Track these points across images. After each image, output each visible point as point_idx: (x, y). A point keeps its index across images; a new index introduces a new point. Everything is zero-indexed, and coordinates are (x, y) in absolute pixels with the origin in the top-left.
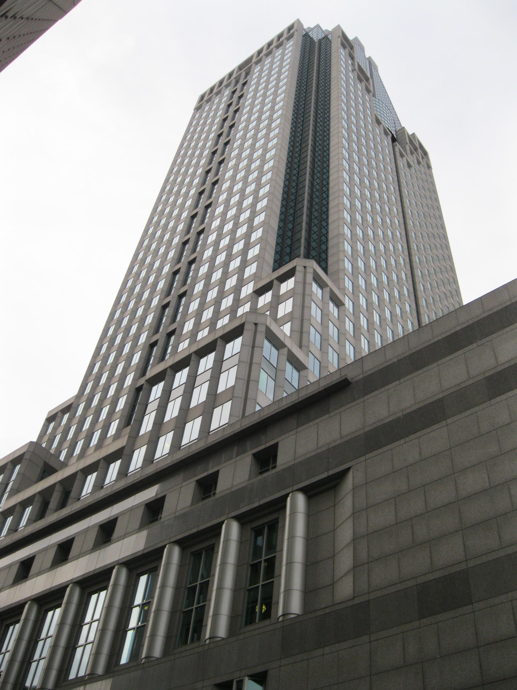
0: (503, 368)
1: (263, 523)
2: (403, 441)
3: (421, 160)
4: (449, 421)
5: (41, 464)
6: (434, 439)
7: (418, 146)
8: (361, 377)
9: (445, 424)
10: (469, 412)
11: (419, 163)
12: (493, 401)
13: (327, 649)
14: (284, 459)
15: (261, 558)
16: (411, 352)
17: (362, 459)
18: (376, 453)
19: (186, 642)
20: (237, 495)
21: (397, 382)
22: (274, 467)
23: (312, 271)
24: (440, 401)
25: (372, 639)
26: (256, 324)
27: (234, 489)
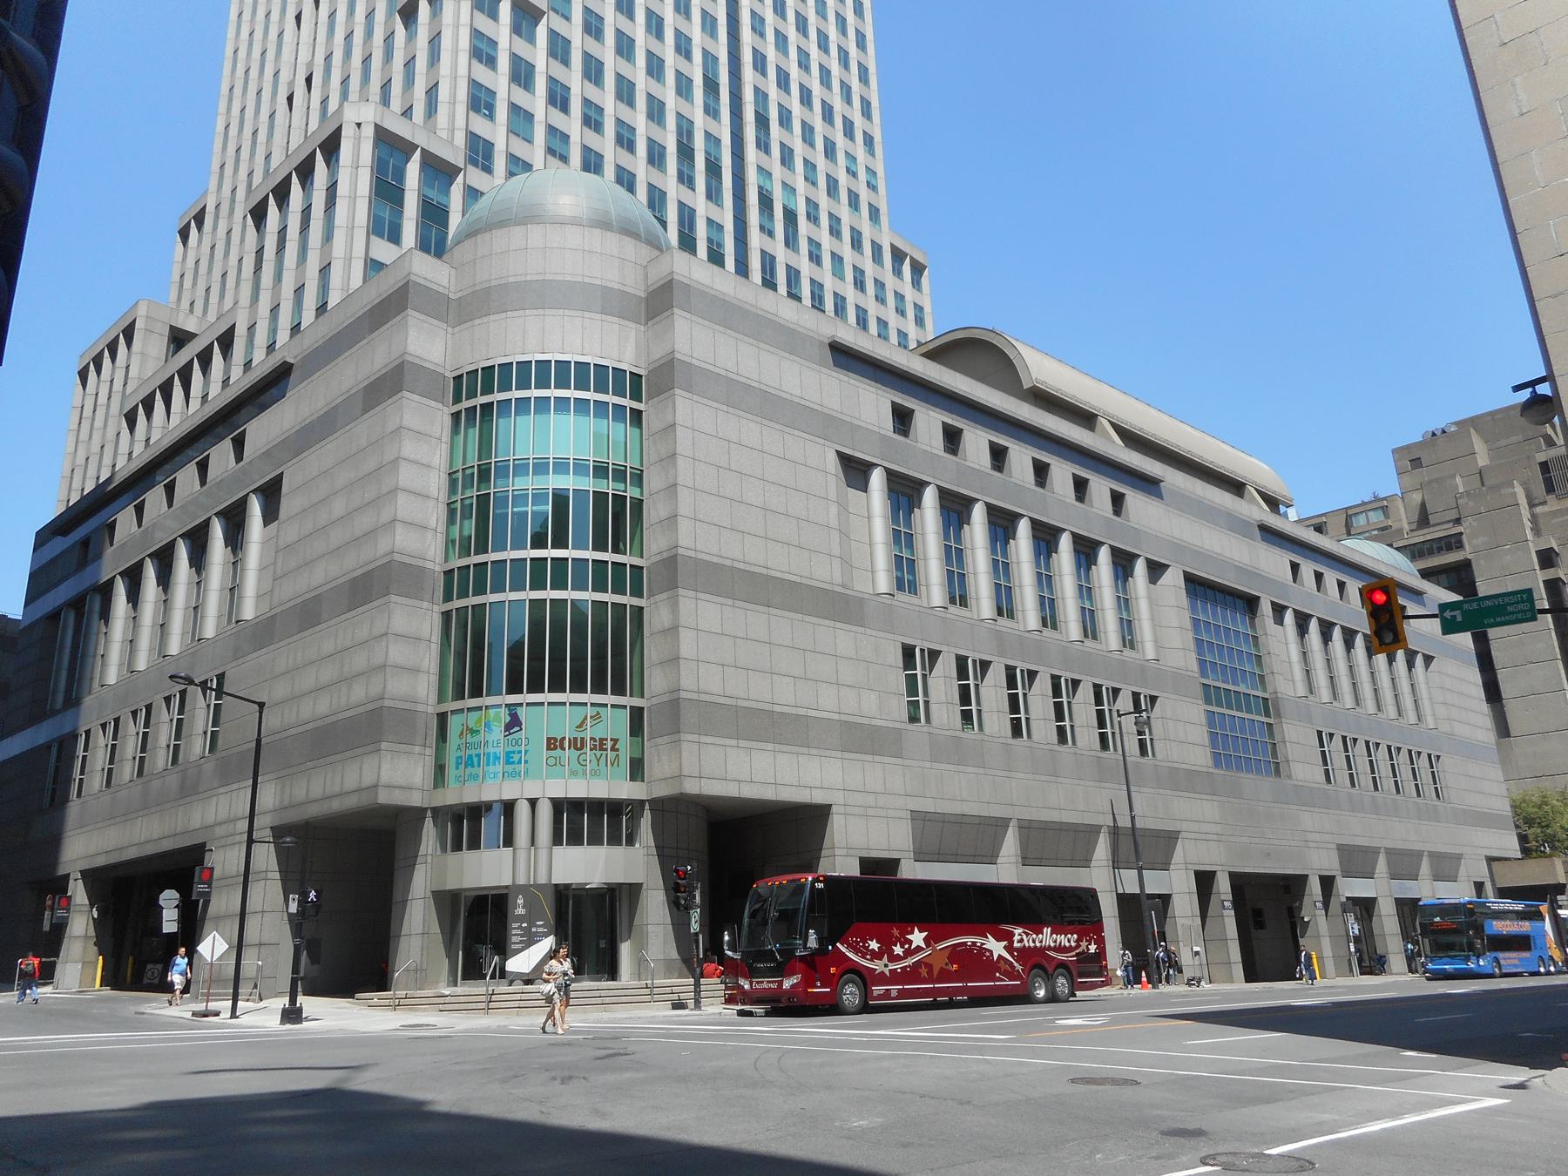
26: (359, 125)
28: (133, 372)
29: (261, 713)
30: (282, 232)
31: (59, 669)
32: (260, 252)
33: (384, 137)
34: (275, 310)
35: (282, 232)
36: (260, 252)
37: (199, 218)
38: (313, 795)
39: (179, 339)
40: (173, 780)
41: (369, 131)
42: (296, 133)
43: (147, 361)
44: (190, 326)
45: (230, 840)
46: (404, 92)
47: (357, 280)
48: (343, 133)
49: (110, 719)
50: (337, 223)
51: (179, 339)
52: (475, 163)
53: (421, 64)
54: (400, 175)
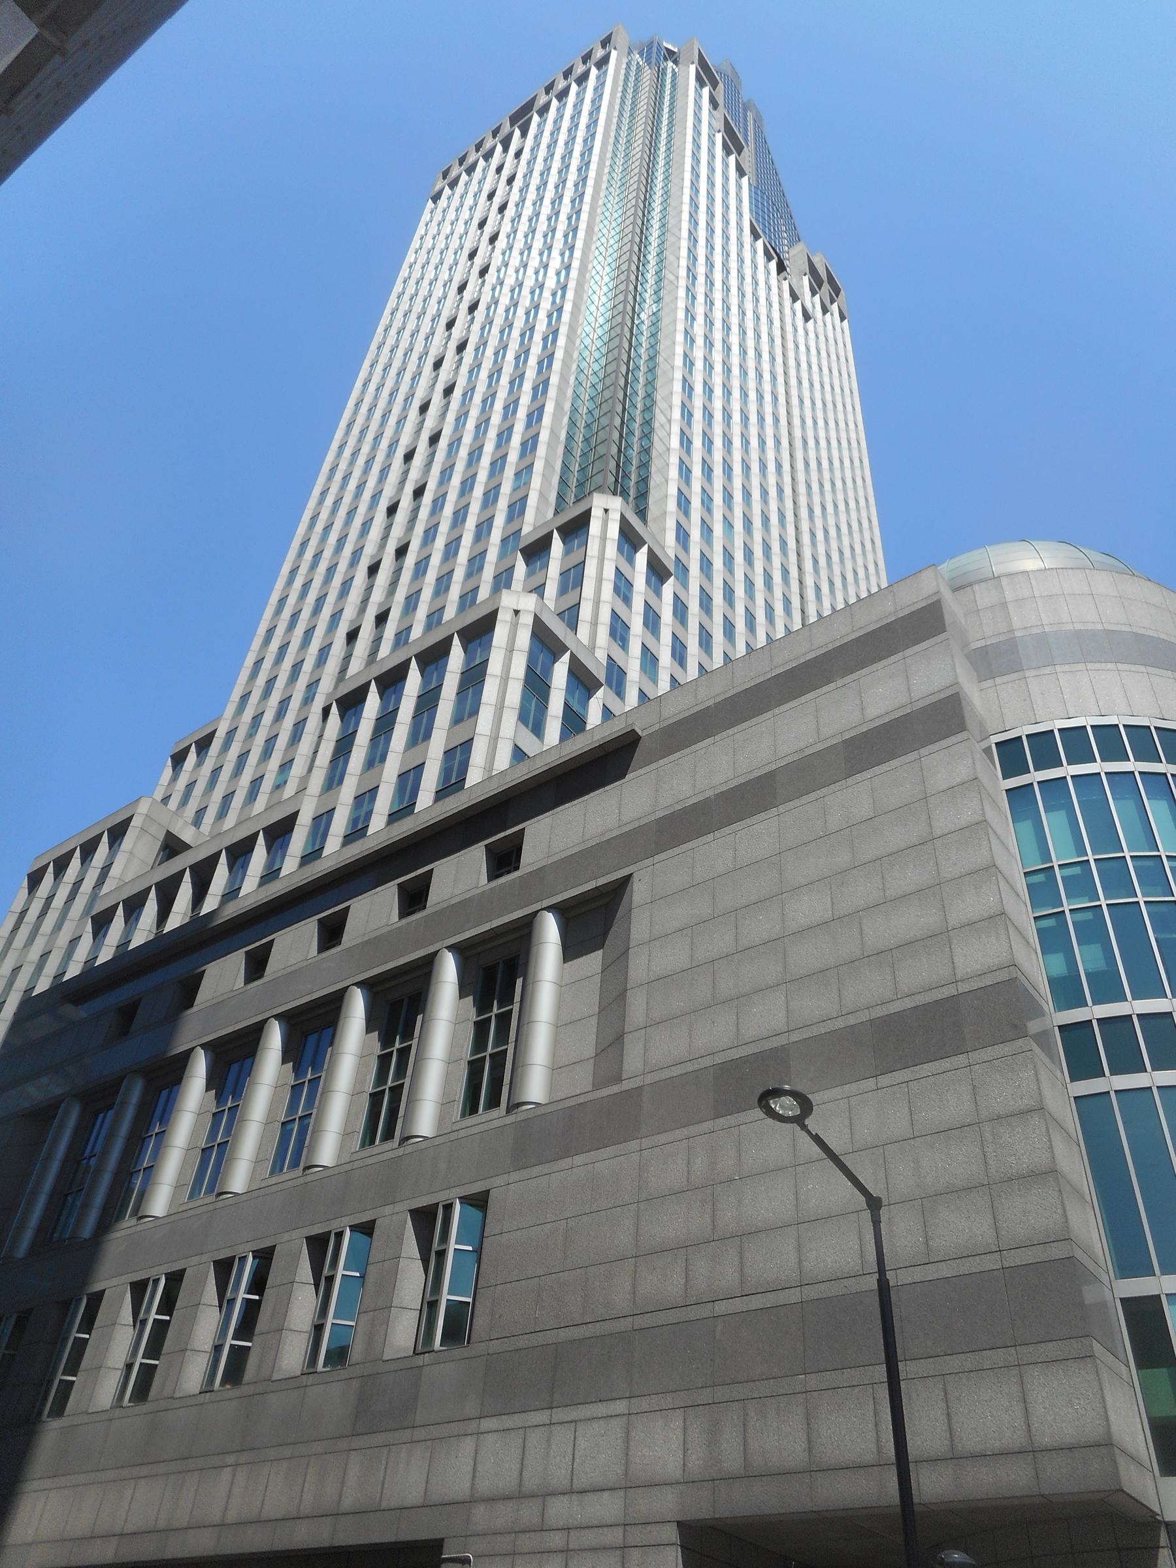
0: (872, 726)
1: (497, 972)
2: (710, 837)
3: (827, 302)
4: (782, 808)
5: (162, 836)
6: (758, 835)
7: (824, 276)
8: (657, 727)
9: (966, 1063)
10: (813, 796)
11: (825, 310)
12: (850, 781)
13: (578, 1160)
14: (531, 857)
15: (486, 1050)
16: (735, 691)
17: (648, 862)
18: (670, 853)
19: (372, 1142)
20: (462, 909)
21: (709, 741)
22: (517, 868)
23: (618, 517)
24: (771, 775)
25: (644, 1146)
26: (517, 612)
27: (454, 901)
28: (115, 871)
29: (876, 1223)
30: (77, 884)
31: (35, 1193)
32: (23, 913)
33: (540, 632)
34: (45, 956)
35: (77, 884)
36: (23, 913)
37: (204, 744)
38: (485, 1486)
39: (172, 847)
40: (333, 1396)
41: (527, 620)
42: (94, 817)
43: (134, 863)
44: (187, 835)
45: (527, 1542)
46: (258, 764)
47: (503, 760)
48: (499, 617)
49: (247, 1250)
50: (484, 699)
51: (172, 847)
52: (610, 686)
53: (253, 758)
54: (548, 670)
